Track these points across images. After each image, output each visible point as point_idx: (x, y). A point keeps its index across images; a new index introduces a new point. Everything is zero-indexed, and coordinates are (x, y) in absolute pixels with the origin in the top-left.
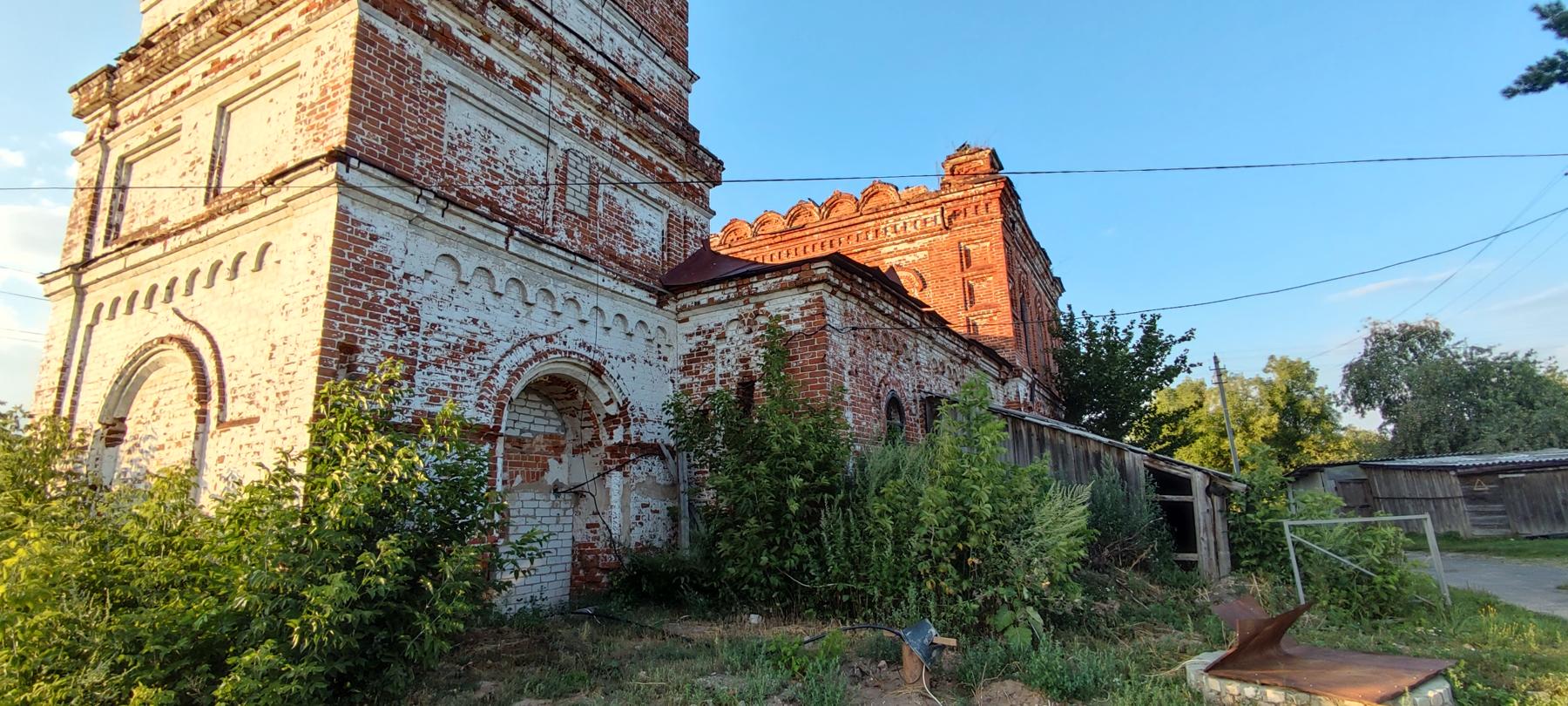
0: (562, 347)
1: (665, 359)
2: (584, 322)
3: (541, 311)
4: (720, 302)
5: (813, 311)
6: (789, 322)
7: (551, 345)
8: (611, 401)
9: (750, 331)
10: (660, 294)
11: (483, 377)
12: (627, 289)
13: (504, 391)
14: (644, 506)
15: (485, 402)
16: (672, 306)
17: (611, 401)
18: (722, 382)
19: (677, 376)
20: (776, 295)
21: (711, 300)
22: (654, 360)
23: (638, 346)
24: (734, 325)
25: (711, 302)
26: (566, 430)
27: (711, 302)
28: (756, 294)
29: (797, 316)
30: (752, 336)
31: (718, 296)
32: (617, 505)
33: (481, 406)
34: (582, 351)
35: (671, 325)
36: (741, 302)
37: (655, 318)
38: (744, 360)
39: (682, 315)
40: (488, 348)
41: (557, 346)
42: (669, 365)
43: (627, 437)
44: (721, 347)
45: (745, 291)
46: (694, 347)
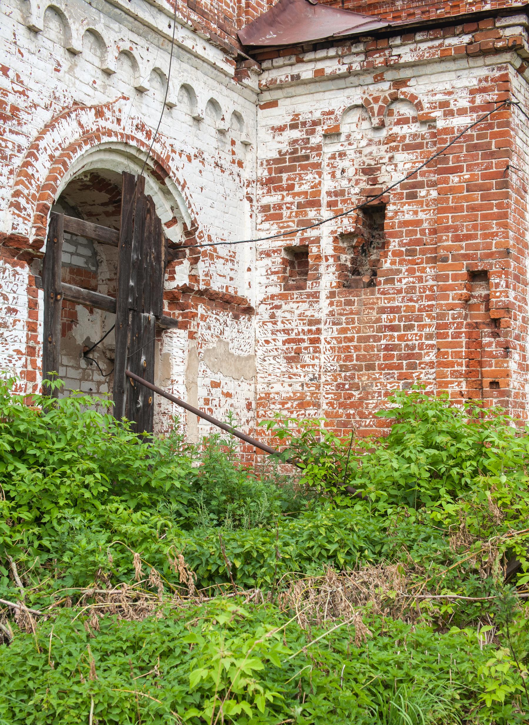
0: (115, 127)
1: (240, 164)
2: (140, 91)
3: (88, 67)
4: (335, 77)
5: (492, 97)
6: (449, 114)
7: (102, 123)
8: (174, 221)
9: (382, 125)
10: (239, 60)
11: (17, 161)
12: (200, 47)
13: (45, 187)
14: (216, 385)
15: (22, 201)
16: (251, 82)
17: (174, 221)
18: (330, 205)
19: (257, 191)
20: (428, 69)
21: (319, 72)
22: (226, 164)
23: (207, 140)
24: (355, 115)
25: (320, 77)
26: (97, 264)
27: (320, 77)
28: (397, 67)
29: (464, 103)
30: (384, 133)
31: (331, 67)
32: (181, 379)
33: (17, 205)
34: (141, 136)
35: (247, 110)
36: (369, 79)
37: (230, 100)
38: (370, 171)
39: (267, 97)
40: (23, 115)
41: (109, 125)
42: (247, 174)
43: (194, 278)
44: (330, 149)
45: (378, 60)
46: (285, 148)
